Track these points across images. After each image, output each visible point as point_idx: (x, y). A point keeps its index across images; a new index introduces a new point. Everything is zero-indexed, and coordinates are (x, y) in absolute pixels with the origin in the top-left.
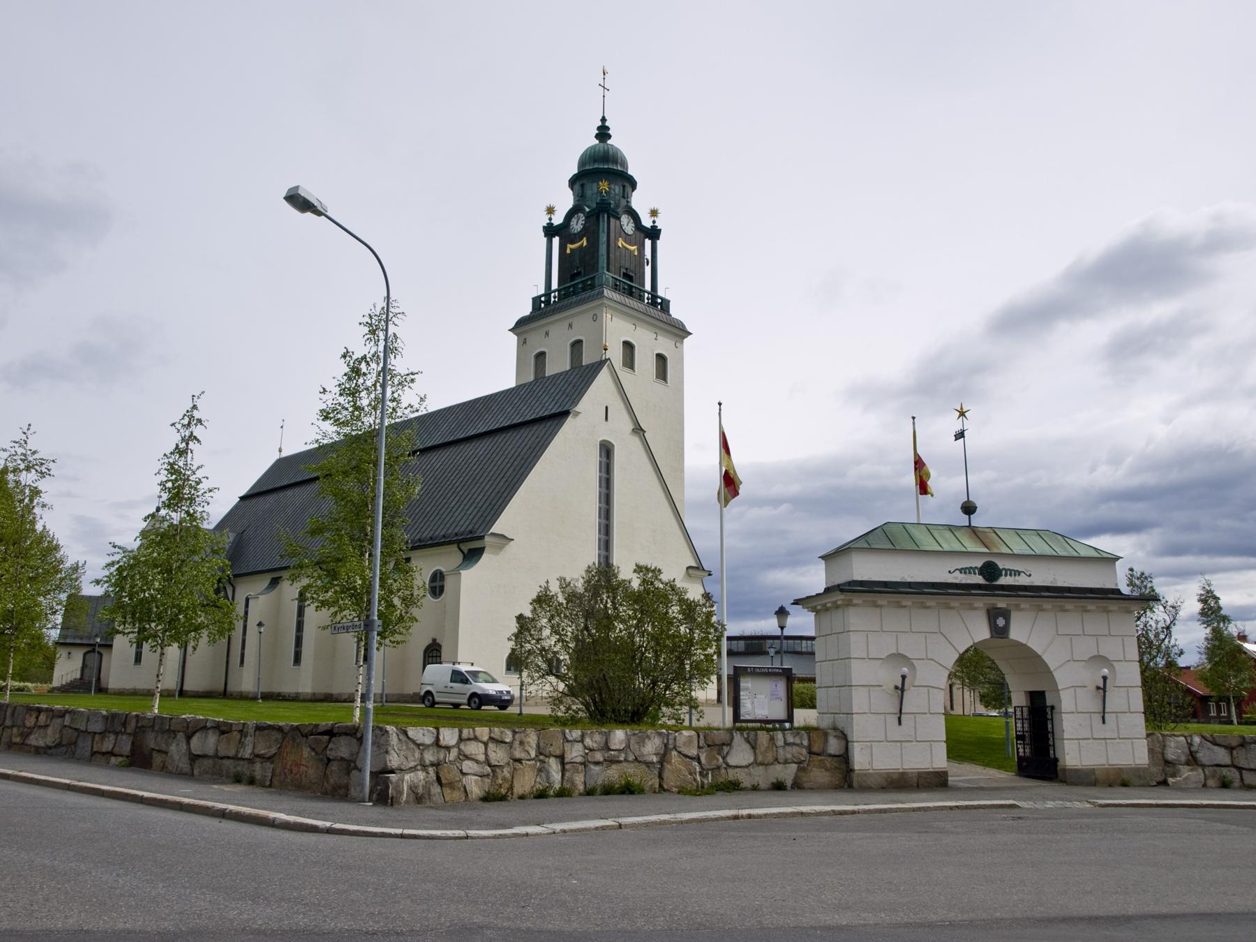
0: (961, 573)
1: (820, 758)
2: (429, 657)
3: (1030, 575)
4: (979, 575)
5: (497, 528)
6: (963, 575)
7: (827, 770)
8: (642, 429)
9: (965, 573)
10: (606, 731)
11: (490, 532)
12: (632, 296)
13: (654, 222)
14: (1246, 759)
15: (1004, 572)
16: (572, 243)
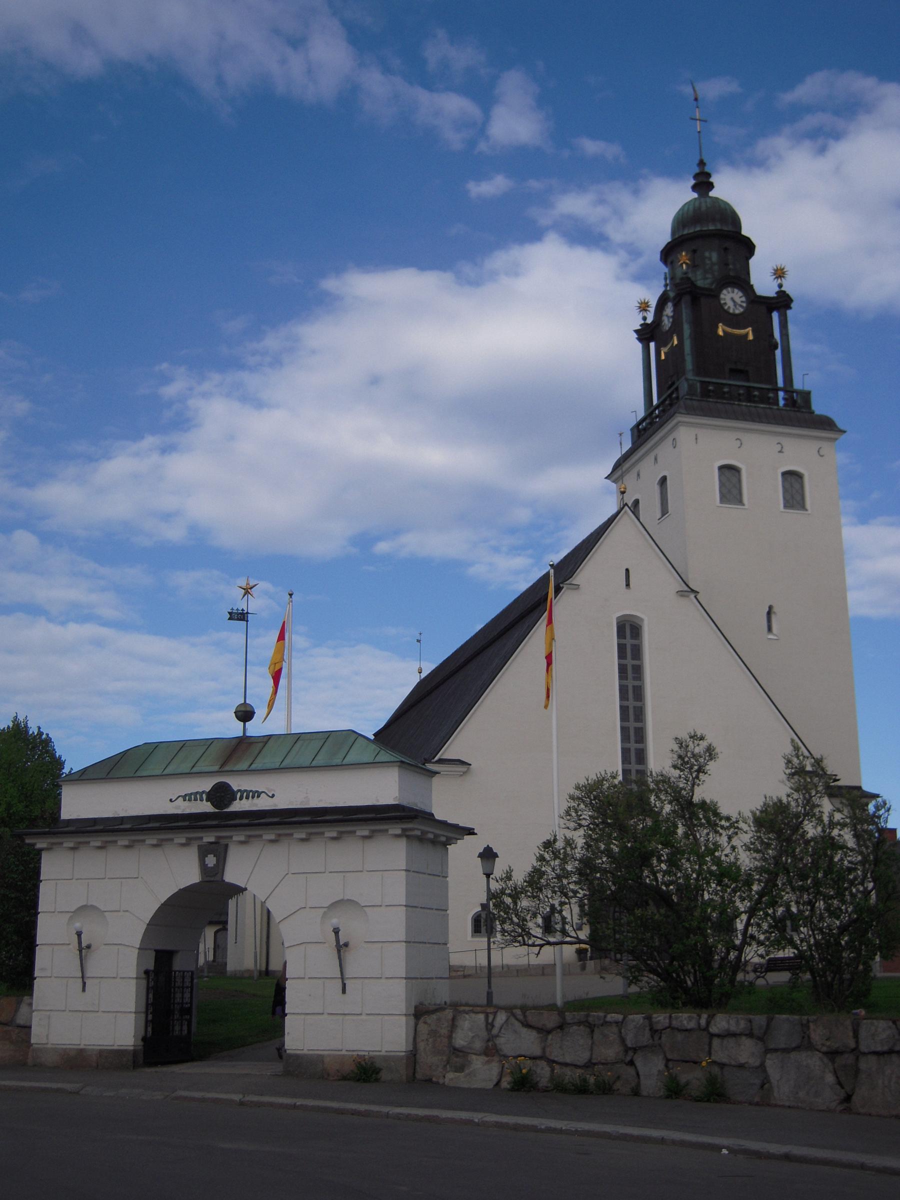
0: (185, 800)
3: (273, 796)
5: (450, 751)
6: (187, 803)
8: (693, 591)
9: (190, 800)
10: (620, 1017)
11: (436, 758)
13: (780, 286)
14: (561, 1047)
15: (239, 795)
16: (665, 346)
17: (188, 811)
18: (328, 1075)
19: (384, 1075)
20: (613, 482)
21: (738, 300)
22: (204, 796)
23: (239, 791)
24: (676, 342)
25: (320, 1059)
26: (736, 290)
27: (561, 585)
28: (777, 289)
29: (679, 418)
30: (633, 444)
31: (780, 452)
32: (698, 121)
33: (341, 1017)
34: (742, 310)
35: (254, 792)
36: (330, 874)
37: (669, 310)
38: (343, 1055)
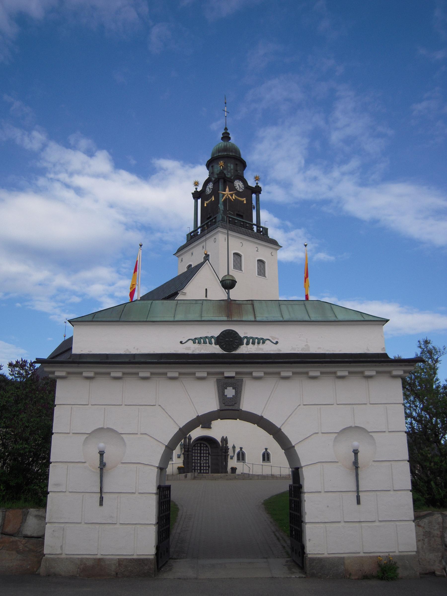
0: (194, 343)
1: (13, 539)
2: (201, 444)
3: (277, 343)
4: (215, 344)
6: (197, 345)
7: (18, 552)
9: (199, 343)
12: (235, 225)
15: (245, 341)
16: (207, 201)
17: (197, 352)
18: (350, 574)
19: (401, 573)
20: (177, 257)
21: (241, 186)
22: (213, 341)
23: (246, 337)
24: (213, 199)
25: (341, 561)
26: (240, 182)
27: (178, 292)
28: (256, 185)
29: (219, 229)
30: (187, 241)
31: (257, 251)
32: (226, 111)
33: (357, 525)
34: (242, 190)
35: (259, 339)
36: (305, 407)
37: (211, 185)
38: (362, 557)
